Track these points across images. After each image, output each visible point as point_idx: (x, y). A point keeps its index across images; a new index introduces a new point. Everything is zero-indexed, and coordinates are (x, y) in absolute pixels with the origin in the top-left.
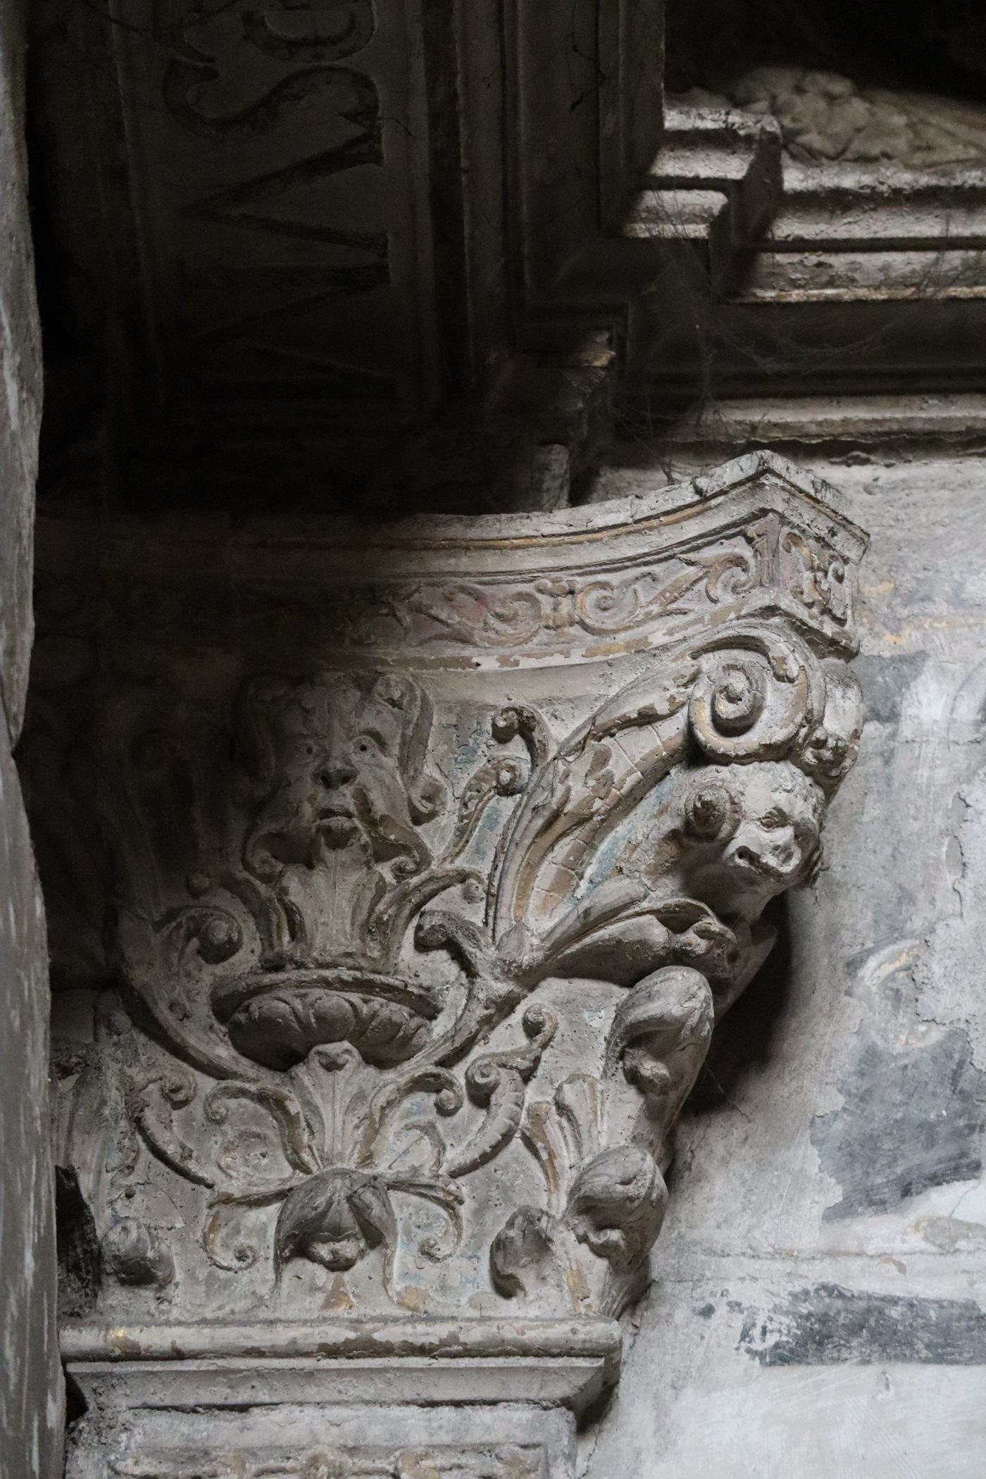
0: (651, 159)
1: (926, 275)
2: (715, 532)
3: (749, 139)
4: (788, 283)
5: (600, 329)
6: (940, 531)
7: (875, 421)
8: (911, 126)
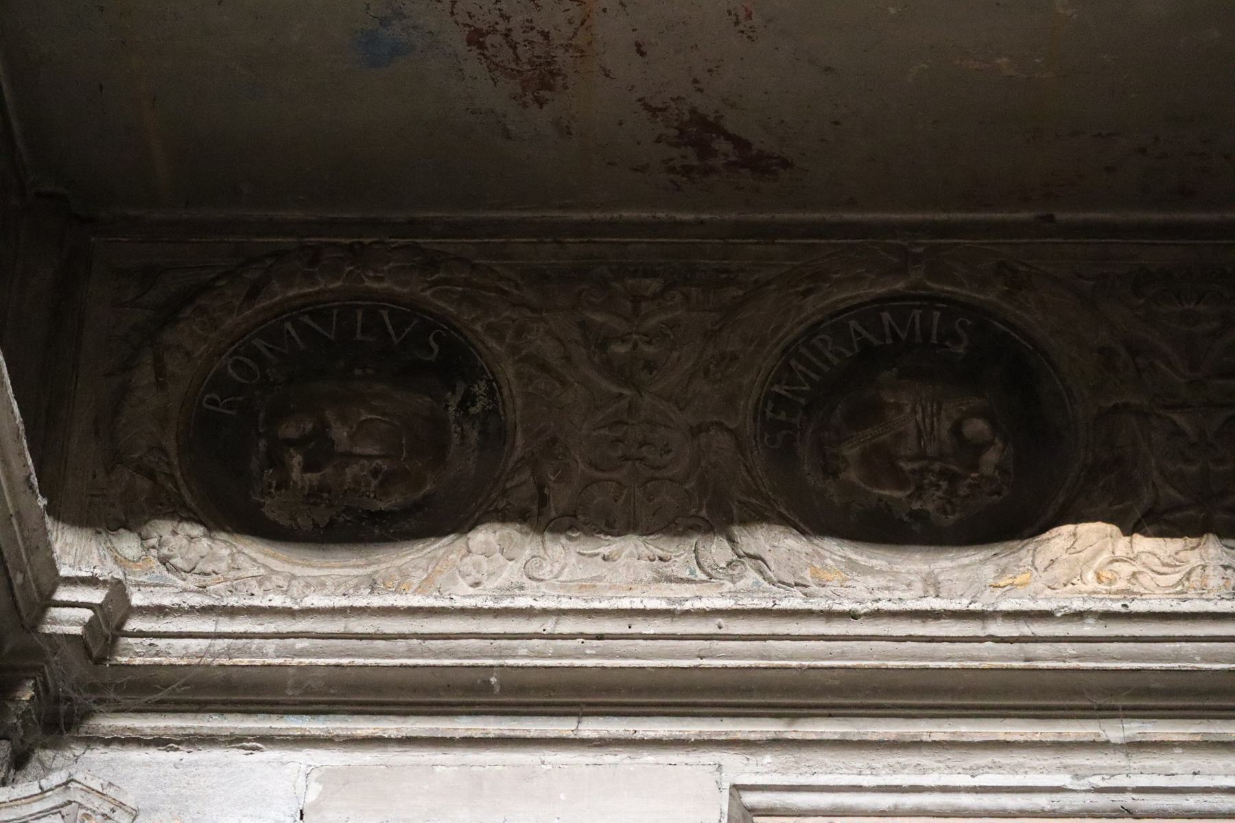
0: (53, 591)
1: (207, 651)
2: (48, 811)
3: (105, 582)
4: (133, 653)
5: (28, 678)
6: (210, 791)
7: (182, 728)
8: (232, 555)
